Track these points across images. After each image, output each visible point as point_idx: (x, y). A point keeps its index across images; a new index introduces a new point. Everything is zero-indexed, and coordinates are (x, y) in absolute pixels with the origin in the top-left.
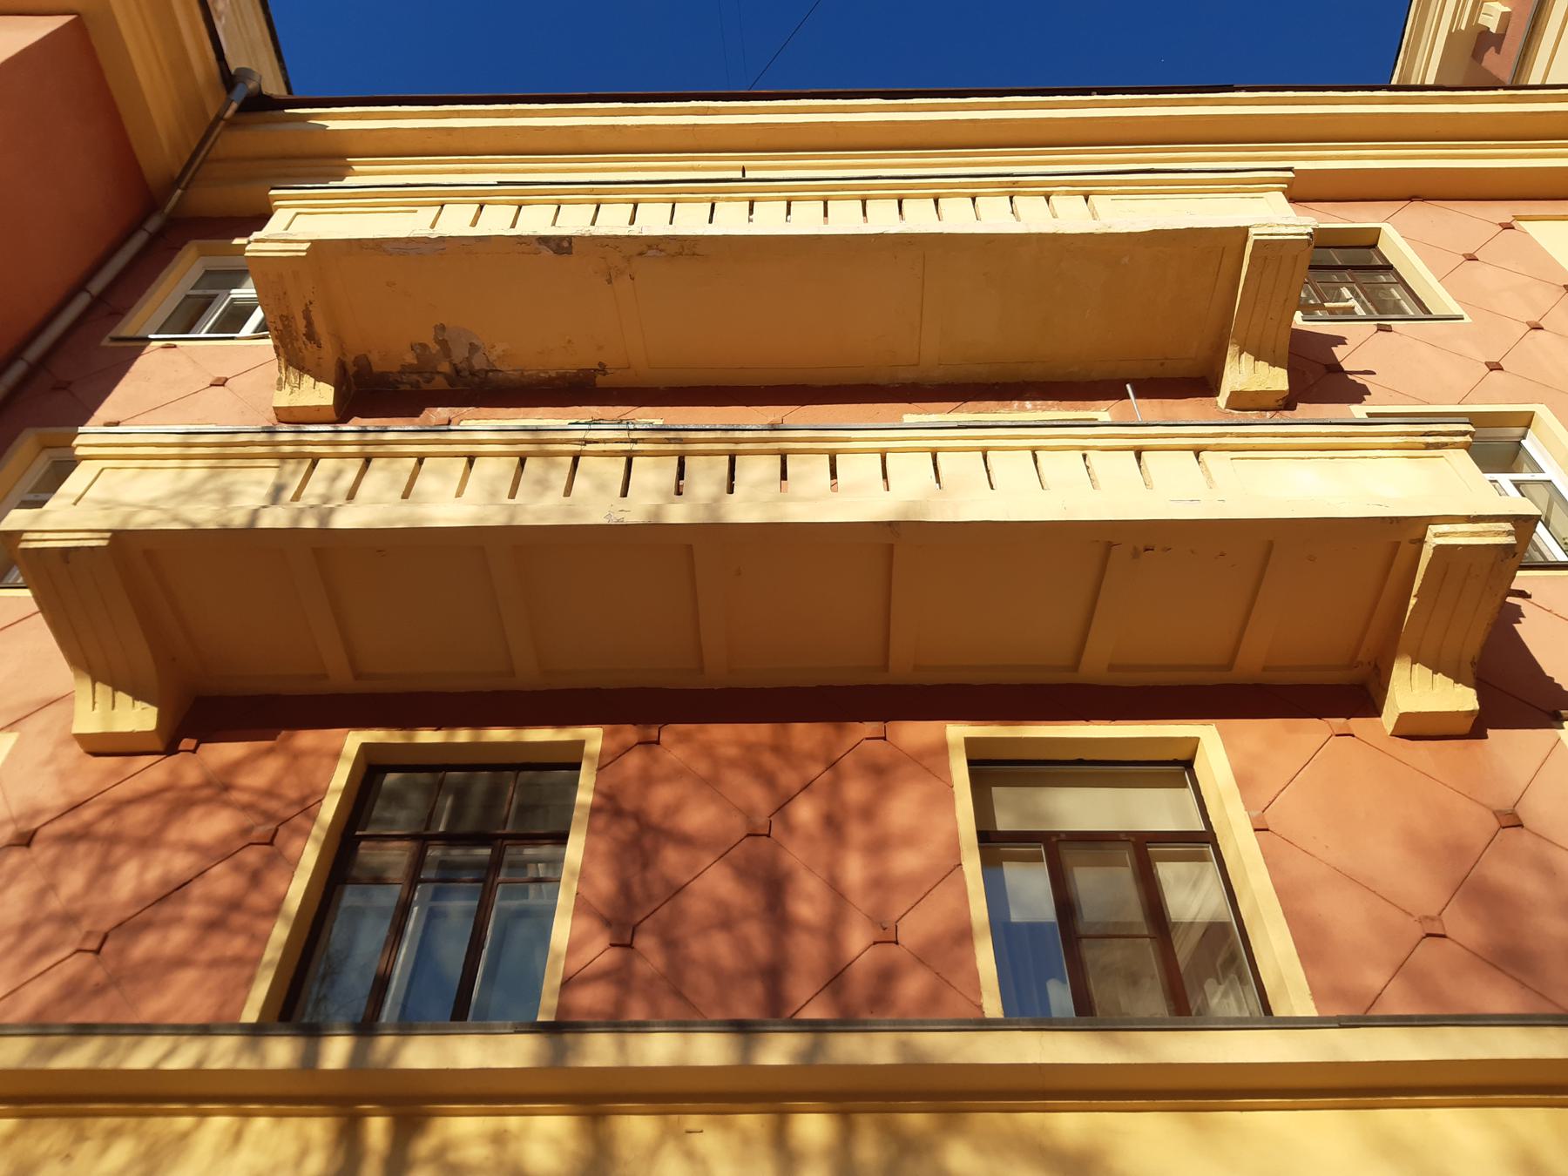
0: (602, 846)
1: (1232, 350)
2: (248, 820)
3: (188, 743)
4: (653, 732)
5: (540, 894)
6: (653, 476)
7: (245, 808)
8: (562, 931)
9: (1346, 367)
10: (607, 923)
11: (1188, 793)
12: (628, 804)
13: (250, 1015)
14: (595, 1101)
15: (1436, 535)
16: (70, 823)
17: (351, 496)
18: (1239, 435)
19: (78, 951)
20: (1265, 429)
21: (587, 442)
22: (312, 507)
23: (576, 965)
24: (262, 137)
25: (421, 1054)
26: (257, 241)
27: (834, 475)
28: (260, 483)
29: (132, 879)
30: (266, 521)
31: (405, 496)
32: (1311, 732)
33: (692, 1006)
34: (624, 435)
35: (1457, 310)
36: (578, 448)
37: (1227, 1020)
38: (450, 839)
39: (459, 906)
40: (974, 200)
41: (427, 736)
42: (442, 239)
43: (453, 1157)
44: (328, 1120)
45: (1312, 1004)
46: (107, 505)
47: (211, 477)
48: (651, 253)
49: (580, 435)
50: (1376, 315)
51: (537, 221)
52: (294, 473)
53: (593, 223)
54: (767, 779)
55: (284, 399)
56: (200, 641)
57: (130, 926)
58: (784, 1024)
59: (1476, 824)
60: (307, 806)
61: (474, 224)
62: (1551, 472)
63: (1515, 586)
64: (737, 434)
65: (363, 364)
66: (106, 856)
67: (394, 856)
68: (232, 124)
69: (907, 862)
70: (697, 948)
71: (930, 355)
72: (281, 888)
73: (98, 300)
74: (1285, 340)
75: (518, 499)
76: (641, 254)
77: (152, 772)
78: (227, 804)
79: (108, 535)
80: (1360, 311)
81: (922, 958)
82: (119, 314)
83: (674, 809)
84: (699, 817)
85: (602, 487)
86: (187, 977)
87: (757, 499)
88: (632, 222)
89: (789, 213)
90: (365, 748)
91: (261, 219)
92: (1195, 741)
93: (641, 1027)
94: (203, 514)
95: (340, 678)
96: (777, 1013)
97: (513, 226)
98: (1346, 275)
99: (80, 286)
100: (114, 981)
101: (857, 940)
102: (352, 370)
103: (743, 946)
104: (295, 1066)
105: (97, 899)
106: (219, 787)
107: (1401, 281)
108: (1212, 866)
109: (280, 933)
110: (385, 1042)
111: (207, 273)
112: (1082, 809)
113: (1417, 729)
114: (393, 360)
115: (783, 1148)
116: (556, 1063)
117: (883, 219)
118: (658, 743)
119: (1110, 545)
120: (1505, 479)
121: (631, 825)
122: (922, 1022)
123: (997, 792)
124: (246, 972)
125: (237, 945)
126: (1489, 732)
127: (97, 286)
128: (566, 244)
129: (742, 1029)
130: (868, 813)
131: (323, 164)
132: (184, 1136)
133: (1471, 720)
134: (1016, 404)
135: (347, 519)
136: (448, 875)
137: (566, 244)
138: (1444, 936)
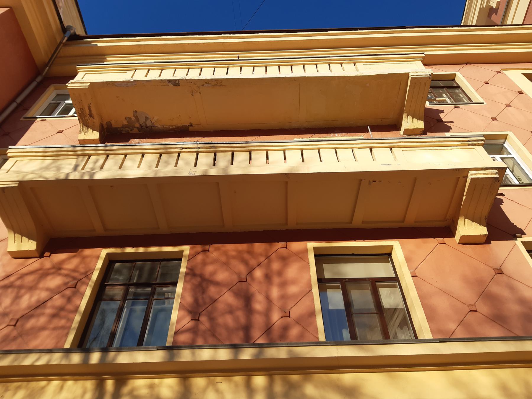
0: (189, 286)
1: (405, 115)
2: (67, 280)
3: (47, 254)
4: (207, 247)
5: (169, 303)
6: (205, 160)
7: (66, 276)
8: (175, 315)
9: (444, 120)
10: (190, 312)
11: (390, 264)
12: (198, 272)
13: (67, 346)
14: (185, 373)
15: (471, 175)
16: (6, 282)
17: (102, 168)
18: (405, 142)
19: (8, 325)
20: (414, 140)
21: (183, 148)
22: (88, 172)
23: (179, 327)
24: (75, 49)
25: (124, 358)
26: (72, 83)
27: (267, 158)
28: (70, 164)
29: (27, 301)
30: (71, 177)
31: (120, 168)
32: (432, 243)
33: (219, 340)
34: (195, 146)
36: (180, 150)
37: (402, 340)
38: (137, 285)
39: (140, 308)
40: (316, 65)
41: (129, 250)
42: (135, 81)
43: (135, 393)
44: (93, 381)
45: (431, 335)
46: (18, 172)
47: (53, 163)
48: (206, 85)
49: (180, 146)
50: (454, 103)
51: (168, 75)
52: (82, 161)
53: (187, 75)
54: (246, 263)
55: (82, 137)
56: (54, 219)
57: (26, 316)
58: (250, 345)
59: (487, 273)
60: (87, 275)
61: (146, 76)
62: (514, 154)
63: (499, 192)
64: (234, 145)
65: (109, 125)
66: (18, 293)
67: (118, 291)
68: (65, 45)
69: (293, 289)
70: (220, 320)
71: (303, 117)
72: (78, 303)
73: (19, 105)
74: (422, 112)
75: (159, 168)
76: (203, 85)
77: (34, 264)
78: (60, 274)
79: (18, 183)
80: (449, 101)
81: (298, 322)
82: (27, 109)
83: (214, 273)
84: (222, 276)
85: (187, 163)
86: (45, 333)
87: (241, 166)
88: (200, 75)
89: (254, 71)
90: (108, 254)
91: (73, 77)
92: (391, 247)
93: (200, 347)
94: (50, 175)
95: (99, 230)
96: (248, 342)
97: (160, 76)
98: (444, 89)
99: (13, 100)
100: (20, 335)
101: (276, 316)
102: (105, 127)
103: (236, 319)
104: (81, 362)
105: (15, 308)
106: (57, 269)
108: (398, 289)
109: (77, 318)
110: (112, 354)
111: (58, 95)
112: (353, 270)
113: (467, 241)
114: (118, 123)
115: (250, 389)
116: (170, 360)
117: (286, 72)
118: (209, 251)
119: (361, 180)
120: (498, 157)
121: (199, 279)
122: (297, 343)
123: (325, 266)
124: (66, 331)
125: (63, 322)
126: (492, 242)
127: (19, 100)
128: (177, 82)
129: (235, 347)
130: (280, 273)
131: (98, 58)
132: (43, 388)
133: (485, 238)
134: (332, 134)
135: (100, 175)
136: (136, 297)
137: (177, 82)
138: (476, 311)
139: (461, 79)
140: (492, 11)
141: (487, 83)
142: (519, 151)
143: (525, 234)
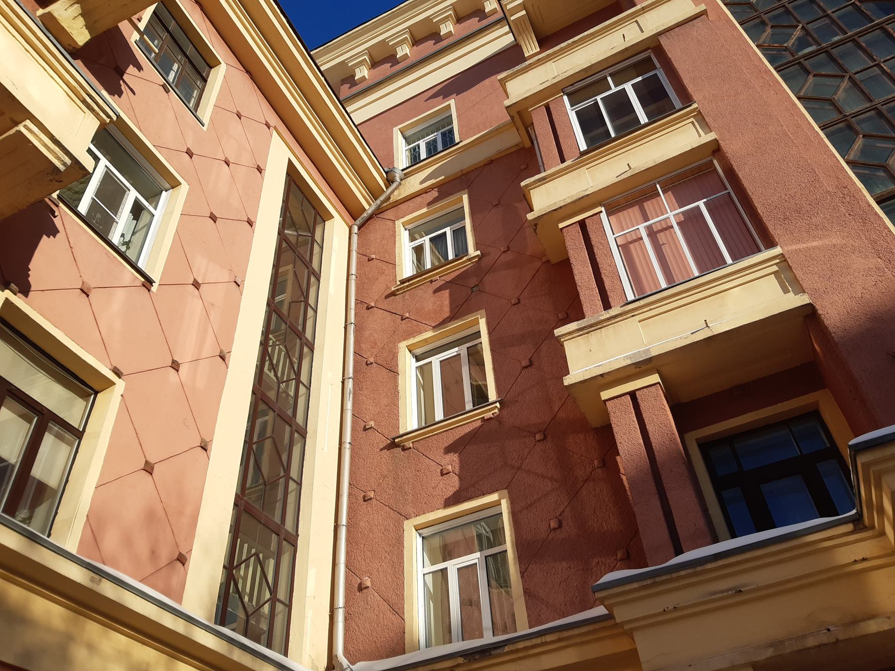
9: (125, 77)
15: (25, 126)
35: (206, 121)
107: (202, 91)
139: (218, 77)
140: (350, 80)
141: (239, 116)
142: (168, 213)
143: (26, 296)
